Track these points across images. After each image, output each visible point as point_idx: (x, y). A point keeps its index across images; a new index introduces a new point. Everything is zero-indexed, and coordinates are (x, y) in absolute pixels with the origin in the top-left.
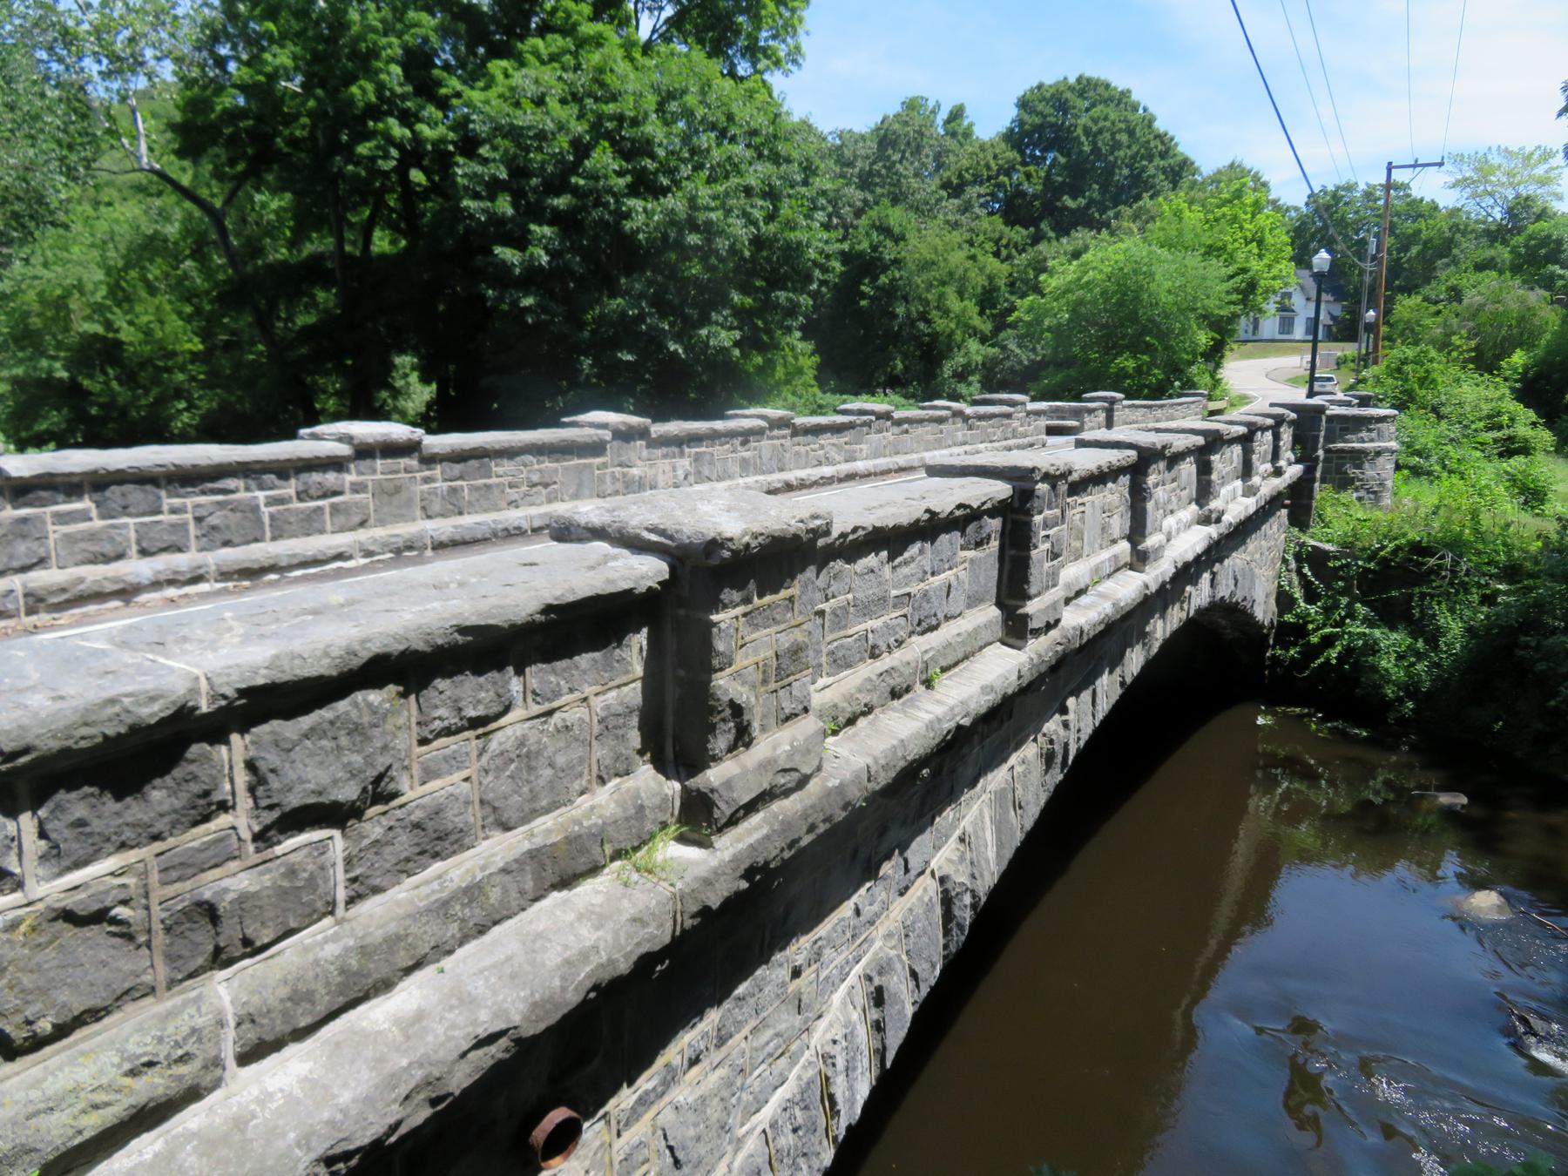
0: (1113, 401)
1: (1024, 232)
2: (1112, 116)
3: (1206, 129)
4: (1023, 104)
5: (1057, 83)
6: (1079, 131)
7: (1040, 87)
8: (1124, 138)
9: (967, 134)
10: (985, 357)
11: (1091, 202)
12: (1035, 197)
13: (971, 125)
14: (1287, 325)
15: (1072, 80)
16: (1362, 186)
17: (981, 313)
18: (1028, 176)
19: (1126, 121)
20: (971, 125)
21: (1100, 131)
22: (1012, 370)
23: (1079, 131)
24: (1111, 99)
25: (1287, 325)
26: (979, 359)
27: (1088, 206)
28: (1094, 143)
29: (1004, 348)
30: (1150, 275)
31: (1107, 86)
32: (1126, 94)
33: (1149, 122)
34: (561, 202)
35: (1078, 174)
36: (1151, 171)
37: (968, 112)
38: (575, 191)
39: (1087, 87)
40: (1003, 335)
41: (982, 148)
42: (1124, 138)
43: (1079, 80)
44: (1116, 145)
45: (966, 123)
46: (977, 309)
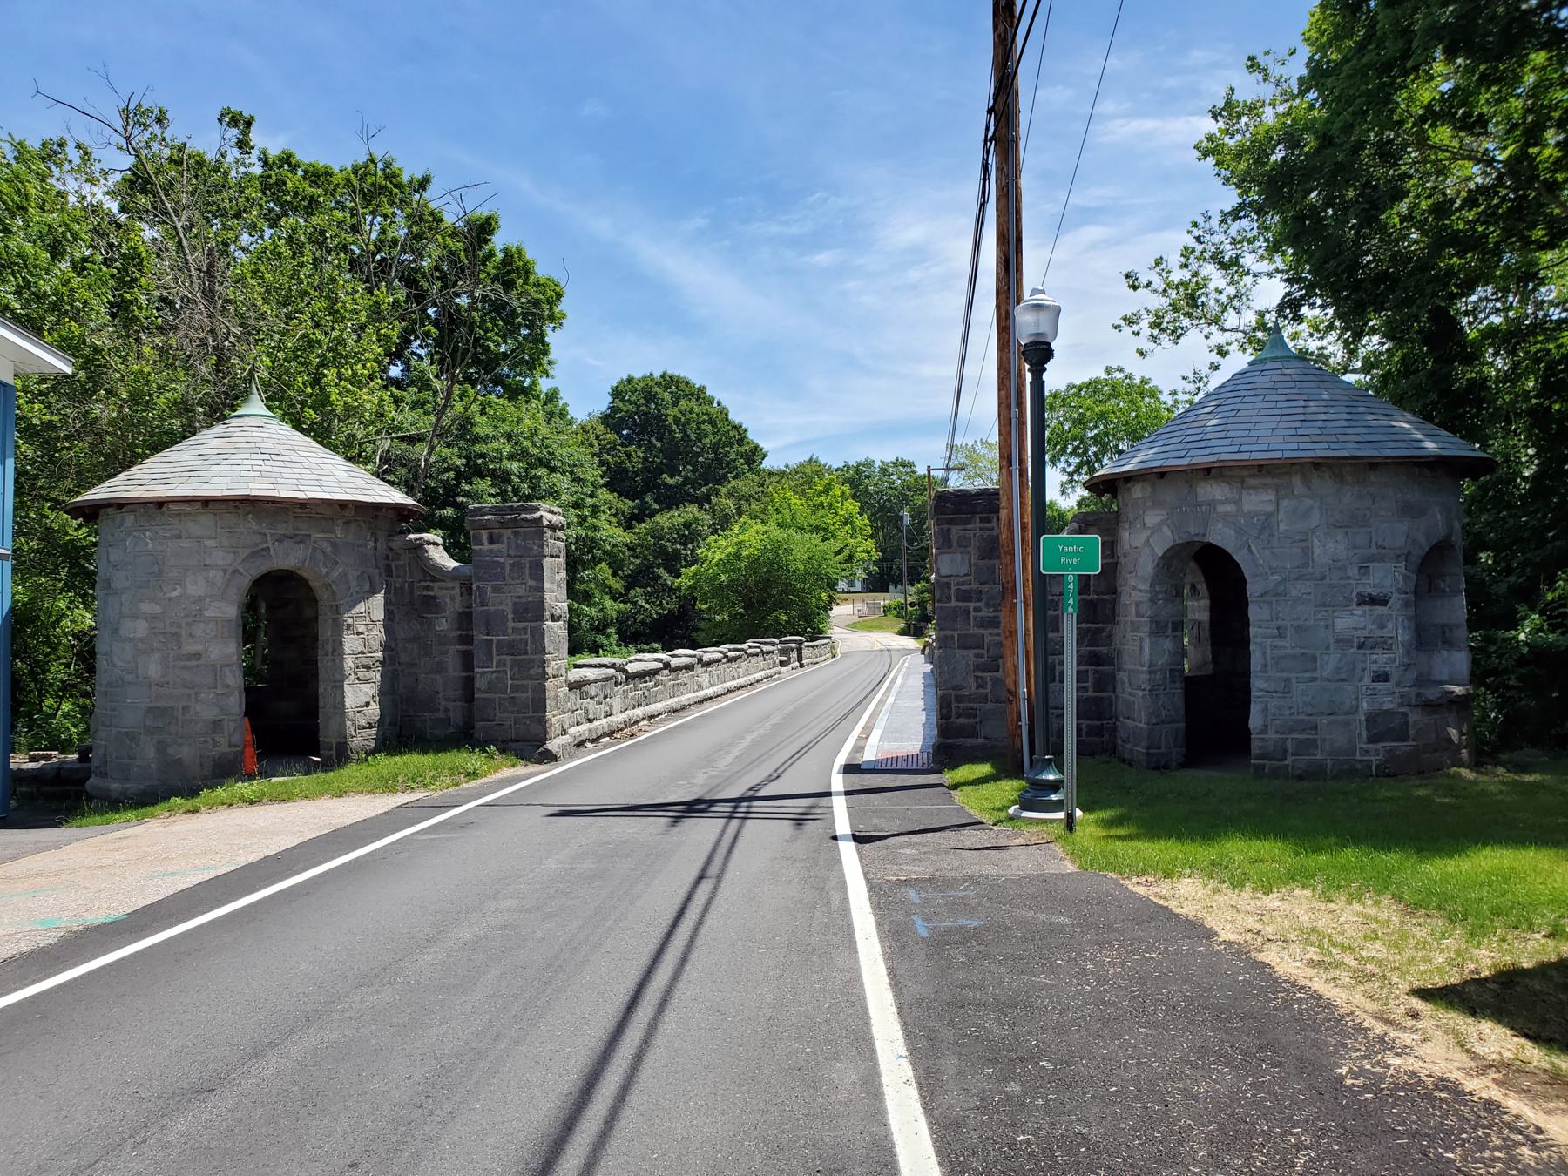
0: (801, 643)
1: (631, 504)
2: (696, 410)
3: (783, 431)
4: (616, 393)
5: (645, 378)
6: (670, 420)
7: (630, 380)
8: (707, 427)
9: (563, 414)
10: (619, 612)
11: (686, 480)
12: (636, 473)
13: (566, 405)
14: (851, 584)
15: (657, 375)
16: (878, 464)
17: (615, 575)
18: (629, 455)
19: (707, 413)
20: (566, 405)
21: (688, 422)
22: (643, 623)
23: (670, 420)
24: (692, 394)
25: (851, 584)
26: (614, 614)
27: (684, 484)
28: (683, 431)
29: (634, 604)
30: (789, 551)
31: (687, 383)
32: (702, 390)
33: (724, 413)
34: (449, 512)
35: (676, 454)
36: (734, 456)
37: (562, 394)
38: (457, 506)
39: (670, 381)
40: (632, 593)
41: (583, 428)
42: (707, 427)
43: (663, 376)
44: (701, 435)
45: (561, 403)
46: (610, 571)
